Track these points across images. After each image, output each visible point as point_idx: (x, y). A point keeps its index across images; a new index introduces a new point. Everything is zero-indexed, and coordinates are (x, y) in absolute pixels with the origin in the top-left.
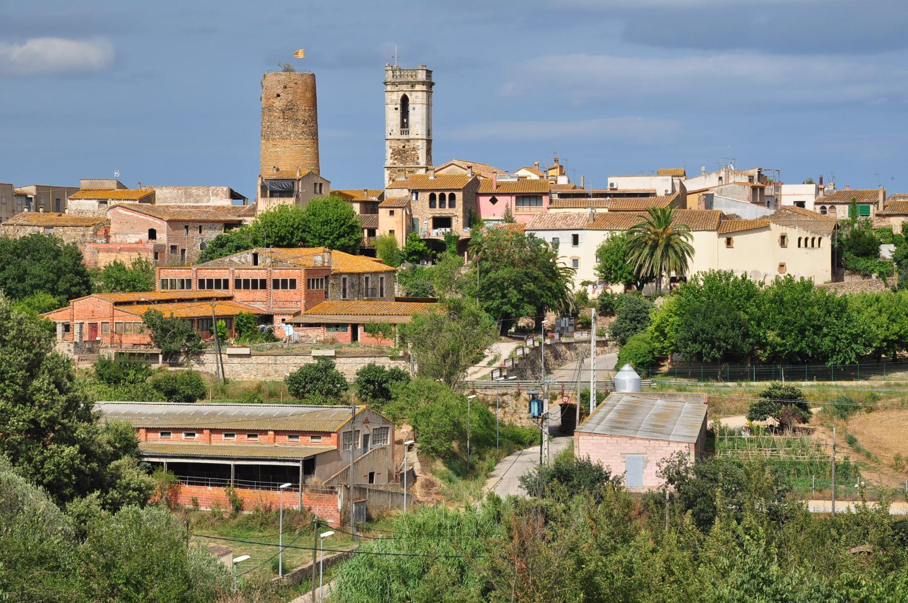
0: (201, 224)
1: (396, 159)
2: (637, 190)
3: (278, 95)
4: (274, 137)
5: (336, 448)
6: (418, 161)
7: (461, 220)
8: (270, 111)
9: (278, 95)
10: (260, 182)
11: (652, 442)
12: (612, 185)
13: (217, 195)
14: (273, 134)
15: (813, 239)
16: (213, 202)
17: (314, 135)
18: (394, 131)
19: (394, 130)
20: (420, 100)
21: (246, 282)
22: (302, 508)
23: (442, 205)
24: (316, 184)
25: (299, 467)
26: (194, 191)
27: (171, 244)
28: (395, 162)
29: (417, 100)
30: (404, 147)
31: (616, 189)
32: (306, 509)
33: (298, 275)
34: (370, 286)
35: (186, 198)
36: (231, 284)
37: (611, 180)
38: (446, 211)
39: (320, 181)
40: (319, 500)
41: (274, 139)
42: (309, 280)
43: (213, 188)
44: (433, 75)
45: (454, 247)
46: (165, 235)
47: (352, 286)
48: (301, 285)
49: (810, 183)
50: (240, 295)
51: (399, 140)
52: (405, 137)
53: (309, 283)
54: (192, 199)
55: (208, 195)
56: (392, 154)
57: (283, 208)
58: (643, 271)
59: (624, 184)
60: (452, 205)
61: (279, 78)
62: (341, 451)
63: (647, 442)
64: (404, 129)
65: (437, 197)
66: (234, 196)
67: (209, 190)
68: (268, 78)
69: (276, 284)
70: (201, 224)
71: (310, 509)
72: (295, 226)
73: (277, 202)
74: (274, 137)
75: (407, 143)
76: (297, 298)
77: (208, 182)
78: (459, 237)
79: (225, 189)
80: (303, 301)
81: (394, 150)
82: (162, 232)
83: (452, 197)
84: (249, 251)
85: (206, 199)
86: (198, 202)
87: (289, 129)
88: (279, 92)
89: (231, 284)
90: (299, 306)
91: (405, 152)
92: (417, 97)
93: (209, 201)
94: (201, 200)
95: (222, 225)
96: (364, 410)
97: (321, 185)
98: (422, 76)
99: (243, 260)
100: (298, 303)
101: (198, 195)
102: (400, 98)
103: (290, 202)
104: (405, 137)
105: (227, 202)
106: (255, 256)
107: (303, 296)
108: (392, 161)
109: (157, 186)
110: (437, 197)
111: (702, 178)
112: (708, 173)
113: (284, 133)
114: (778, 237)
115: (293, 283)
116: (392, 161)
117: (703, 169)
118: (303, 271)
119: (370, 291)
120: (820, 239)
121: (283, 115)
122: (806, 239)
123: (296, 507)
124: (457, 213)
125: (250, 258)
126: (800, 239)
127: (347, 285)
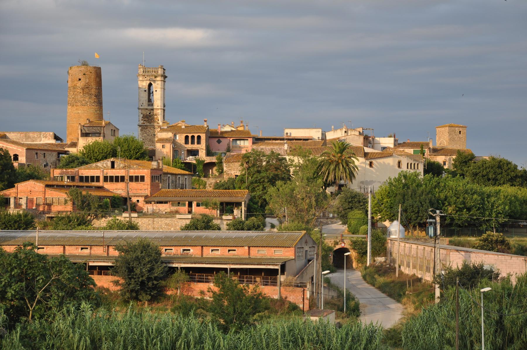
0: (45, 152)
1: (145, 120)
2: (301, 137)
3: (80, 80)
4: (77, 104)
5: (294, 258)
6: (159, 122)
7: (204, 151)
8: (74, 88)
9: (80, 80)
10: (80, 127)
11: (500, 256)
12: (287, 134)
13: (46, 137)
14: (76, 103)
15: (414, 164)
16: (43, 141)
17: (99, 103)
18: (144, 104)
19: (144, 103)
20: (160, 86)
21: (111, 178)
22: (281, 297)
23: (193, 143)
24: (112, 130)
25: (278, 270)
26: (31, 135)
27: (28, 163)
28: (145, 122)
29: (157, 86)
30: (150, 113)
31: (290, 136)
32: (284, 298)
33: (145, 172)
34: (181, 183)
35: (26, 139)
36: (102, 179)
37: (287, 131)
38: (195, 146)
39: (114, 129)
40: (292, 291)
41: (77, 106)
42: (152, 176)
43: (44, 133)
44: (166, 71)
45: (201, 167)
46: (25, 158)
47: (173, 182)
48: (148, 180)
49: (390, 137)
50: (108, 186)
51: (147, 109)
52: (150, 107)
53: (153, 178)
54: (30, 140)
55: (40, 137)
56: (142, 117)
57: (96, 143)
58: (330, 178)
59: (296, 133)
60: (199, 142)
61: (80, 69)
62: (297, 259)
63: (496, 256)
64: (150, 103)
65: (190, 138)
66: (56, 138)
67: (41, 134)
68: (73, 69)
69: (131, 179)
70: (45, 152)
71: (286, 298)
72: (108, 153)
73: (91, 140)
74: (77, 104)
75: (152, 111)
76: (146, 187)
77: (40, 130)
78: (204, 161)
79: (51, 133)
80: (149, 189)
81: (143, 115)
82: (22, 156)
83: (199, 137)
84: (109, 160)
85: (39, 140)
86: (33, 141)
87: (87, 100)
88: (80, 77)
89: (102, 179)
90: (146, 192)
91: (150, 116)
92: (158, 84)
93: (41, 141)
94: (36, 140)
95: (56, 153)
96: (305, 234)
97: (114, 130)
98: (160, 72)
99: (105, 165)
100: (146, 190)
101: (34, 137)
102: (147, 85)
103: (100, 139)
104: (150, 107)
105: (53, 141)
106: (113, 164)
107: (149, 186)
108: (142, 122)
109: (7, 132)
110: (190, 138)
111: (332, 132)
112: (336, 129)
113: (84, 102)
114: (397, 162)
115: (142, 178)
116: (142, 122)
117: (333, 127)
118: (149, 171)
119: (180, 185)
120: (418, 164)
121: (83, 91)
122: (411, 164)
123: (276, 297)
124: (202, 148)
125: (109, 164)
126: (408, 164)
127: (170, 181)
